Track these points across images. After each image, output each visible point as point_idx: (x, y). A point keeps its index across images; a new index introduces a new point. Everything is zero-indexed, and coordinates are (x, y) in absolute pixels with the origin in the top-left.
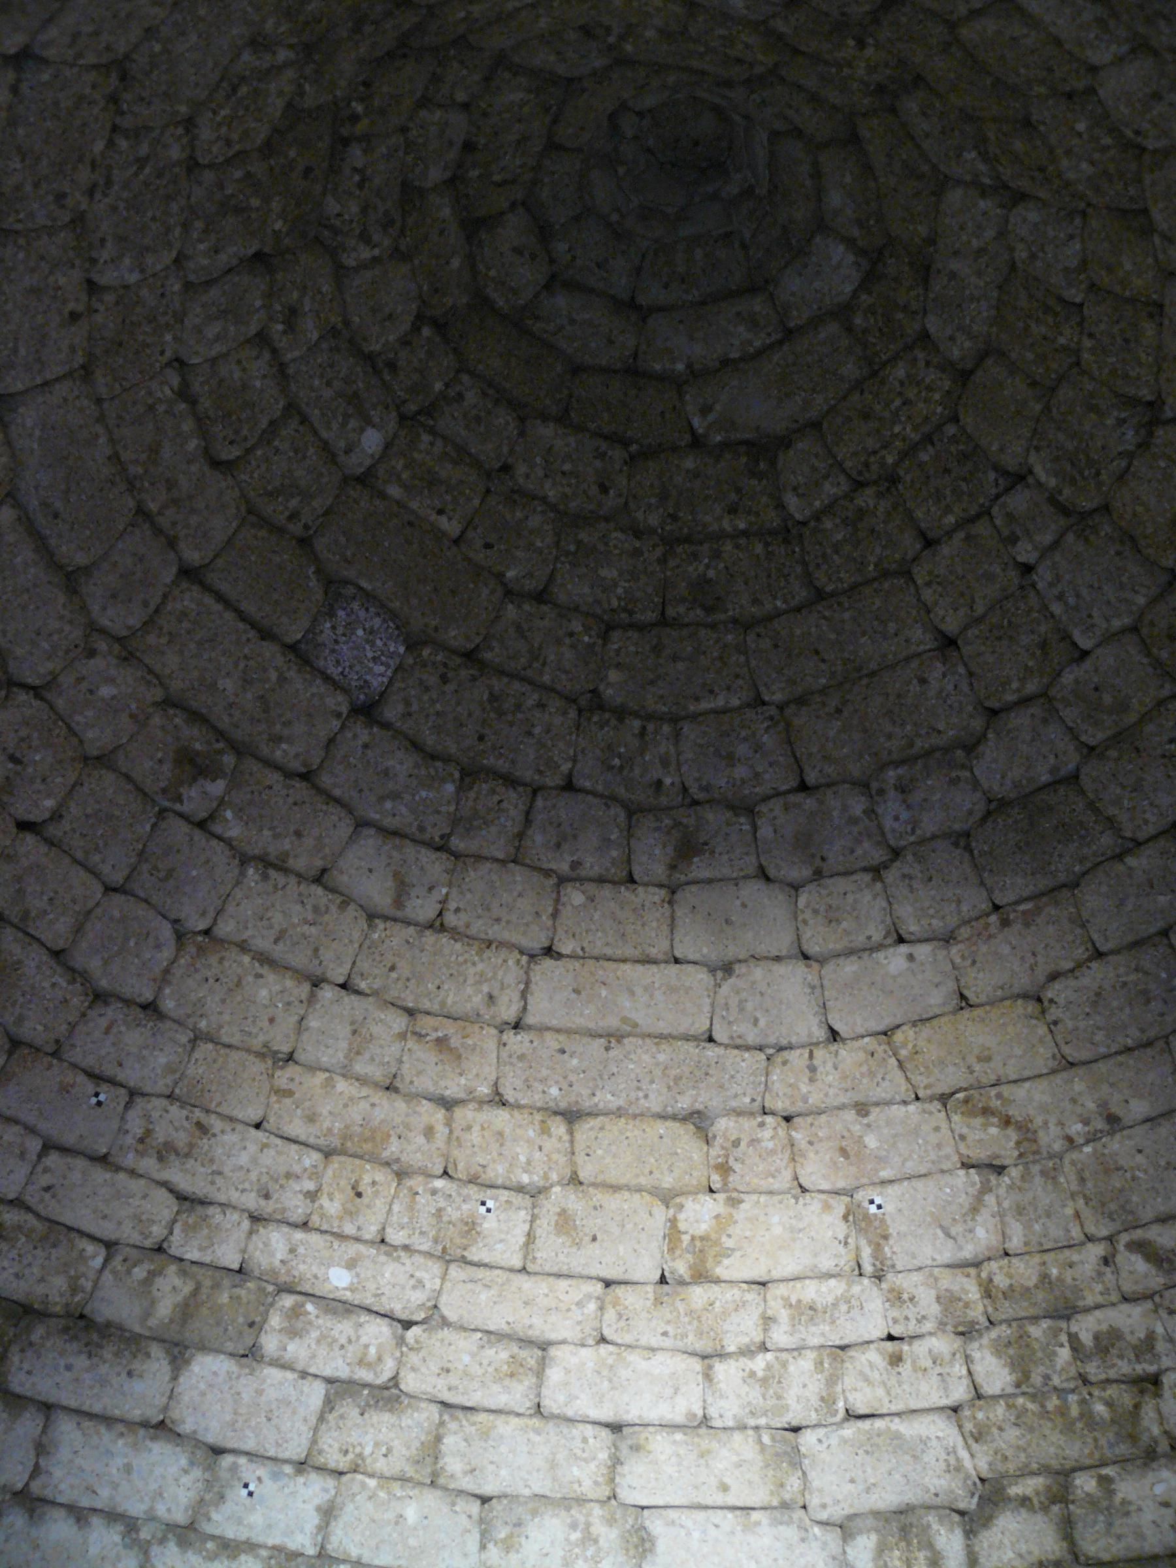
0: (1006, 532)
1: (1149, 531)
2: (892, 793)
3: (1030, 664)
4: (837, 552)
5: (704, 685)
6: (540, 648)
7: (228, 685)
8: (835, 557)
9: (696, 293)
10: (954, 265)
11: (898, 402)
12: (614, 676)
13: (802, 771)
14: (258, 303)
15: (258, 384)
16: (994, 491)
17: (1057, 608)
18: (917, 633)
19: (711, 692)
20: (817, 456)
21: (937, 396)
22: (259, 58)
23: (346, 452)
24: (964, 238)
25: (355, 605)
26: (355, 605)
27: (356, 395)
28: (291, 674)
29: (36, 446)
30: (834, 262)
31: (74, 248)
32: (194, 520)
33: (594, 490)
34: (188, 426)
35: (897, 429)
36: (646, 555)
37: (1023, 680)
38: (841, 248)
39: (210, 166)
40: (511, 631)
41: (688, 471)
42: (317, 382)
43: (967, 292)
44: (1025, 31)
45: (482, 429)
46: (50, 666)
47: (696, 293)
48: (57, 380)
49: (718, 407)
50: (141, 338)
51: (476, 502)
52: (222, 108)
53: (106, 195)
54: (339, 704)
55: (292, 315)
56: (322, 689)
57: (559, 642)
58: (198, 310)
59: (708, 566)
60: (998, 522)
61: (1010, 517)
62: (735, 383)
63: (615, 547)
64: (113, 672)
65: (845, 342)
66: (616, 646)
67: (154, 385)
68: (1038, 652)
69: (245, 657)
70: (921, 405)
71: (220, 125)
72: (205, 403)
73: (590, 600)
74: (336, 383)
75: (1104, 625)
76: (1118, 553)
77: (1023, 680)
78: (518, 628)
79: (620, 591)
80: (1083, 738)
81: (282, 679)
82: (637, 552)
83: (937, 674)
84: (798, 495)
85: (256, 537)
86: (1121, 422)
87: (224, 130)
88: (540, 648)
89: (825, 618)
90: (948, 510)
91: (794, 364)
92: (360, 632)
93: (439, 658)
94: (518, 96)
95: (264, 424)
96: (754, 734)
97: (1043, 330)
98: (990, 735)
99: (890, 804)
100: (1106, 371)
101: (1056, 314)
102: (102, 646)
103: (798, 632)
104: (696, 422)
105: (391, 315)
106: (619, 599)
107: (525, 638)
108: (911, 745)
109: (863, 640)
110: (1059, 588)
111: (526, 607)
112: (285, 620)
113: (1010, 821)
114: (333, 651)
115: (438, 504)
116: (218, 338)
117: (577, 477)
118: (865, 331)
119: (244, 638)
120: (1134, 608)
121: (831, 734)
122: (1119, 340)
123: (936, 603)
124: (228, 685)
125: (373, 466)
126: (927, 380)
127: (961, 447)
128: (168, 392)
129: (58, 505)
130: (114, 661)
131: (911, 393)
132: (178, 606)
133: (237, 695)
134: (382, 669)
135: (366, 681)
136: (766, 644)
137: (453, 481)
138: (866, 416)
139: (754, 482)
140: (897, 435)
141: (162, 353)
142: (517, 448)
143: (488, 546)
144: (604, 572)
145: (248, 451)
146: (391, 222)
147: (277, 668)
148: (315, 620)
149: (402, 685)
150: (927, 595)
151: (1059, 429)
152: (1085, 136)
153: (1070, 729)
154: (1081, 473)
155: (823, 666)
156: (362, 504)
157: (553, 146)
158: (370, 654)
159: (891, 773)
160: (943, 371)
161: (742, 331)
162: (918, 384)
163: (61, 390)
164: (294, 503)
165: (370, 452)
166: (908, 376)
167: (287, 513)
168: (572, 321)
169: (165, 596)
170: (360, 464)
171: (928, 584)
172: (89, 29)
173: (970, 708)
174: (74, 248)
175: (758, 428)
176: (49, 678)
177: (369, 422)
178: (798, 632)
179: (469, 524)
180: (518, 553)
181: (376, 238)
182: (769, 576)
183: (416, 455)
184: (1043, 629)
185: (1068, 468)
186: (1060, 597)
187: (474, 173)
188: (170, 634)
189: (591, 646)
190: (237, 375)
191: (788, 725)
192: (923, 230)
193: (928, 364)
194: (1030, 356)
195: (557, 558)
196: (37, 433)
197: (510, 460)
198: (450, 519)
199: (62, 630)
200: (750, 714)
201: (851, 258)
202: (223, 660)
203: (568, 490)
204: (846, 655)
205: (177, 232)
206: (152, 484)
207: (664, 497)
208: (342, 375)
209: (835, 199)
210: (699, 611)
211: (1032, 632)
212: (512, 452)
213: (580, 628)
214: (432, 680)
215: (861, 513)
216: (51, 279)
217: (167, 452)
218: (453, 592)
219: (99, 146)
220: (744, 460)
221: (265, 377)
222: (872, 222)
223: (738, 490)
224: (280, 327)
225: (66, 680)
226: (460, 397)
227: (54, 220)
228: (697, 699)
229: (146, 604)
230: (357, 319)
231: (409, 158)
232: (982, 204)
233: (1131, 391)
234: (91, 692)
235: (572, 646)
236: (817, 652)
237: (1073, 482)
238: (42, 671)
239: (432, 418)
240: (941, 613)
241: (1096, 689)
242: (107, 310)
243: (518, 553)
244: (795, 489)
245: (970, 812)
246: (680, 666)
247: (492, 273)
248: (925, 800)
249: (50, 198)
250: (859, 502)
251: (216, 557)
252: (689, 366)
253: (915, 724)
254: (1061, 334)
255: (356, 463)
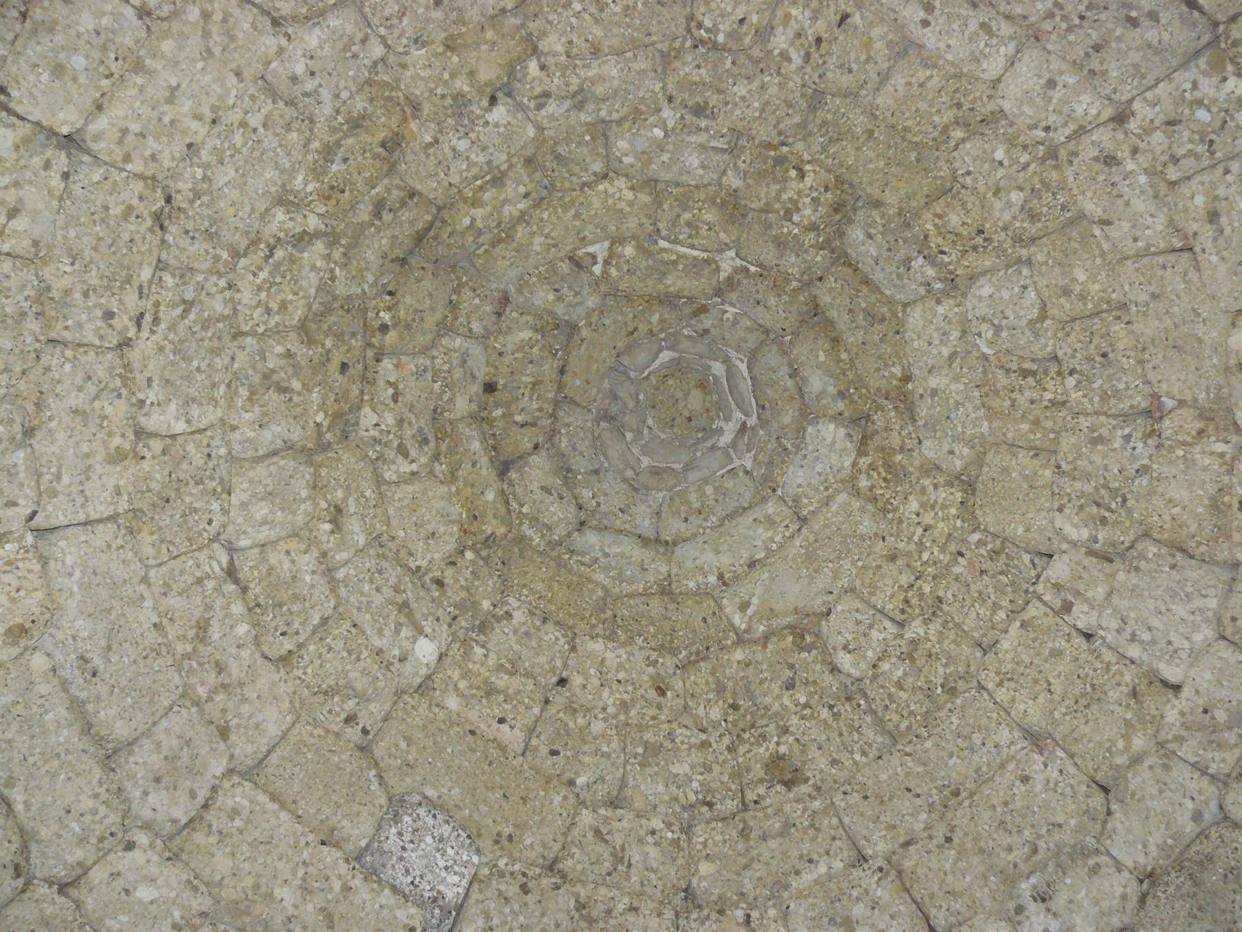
0: (1058, 604)
1: (1193, 528)
2: (1032, 907)
3: (1129, 716)
4: (902, 689)
5: (801, 857)
6: (623, 848)
7: (287, 895)
8: (901, 694)
9: (714, 519)
10: (933, 382)
11: (919, 531)
12: (705, 868)
13: (927, 919)
14: (304, 494)
15: (308, 578)
16: (1033, 573)
17: (1134, 651)
18: (1004, 735)
19: (810, 861)
20: (857, 611)
21: (953, 511)
22: (291, 219)
23: (400, 660)
24: (935, 351)
25: (422, 811)
26: (422, 811)
27: (405, 604)
28: (357, 882)
29: (75, 588)
30: (829, 440)
31: (120, 376)
32: (246, 709)
33: (652, 694)
34: (237, 609)
35: (925, 556)
36: (714, 745)
37: (1126, 737)
38: (832, 426)
39: (252, 333)
40: (590, 835)
41: (739, 662)
42: (366, 587)
43: (952, 401)
44: (928, 73)
45: (534, 644)
46: (79, 854)
47: (714, 519)
48: (99, 521)
49: (755, 601)
50: (188, 499)
51: (536, 710)
52: (261, 269)
53: (153, 332)
54: (412, 917)
55: (337, 514)
56: (392, 901)
57: (641, 841)
58: (245, 485)
59: (778, 744)
60: (1047, 598)
61: (1057, 587)
62: (766, 575)
63: (682, 743)
64: (153, 870)
65: (856, 504)
66: (701, 839)
67: (202, 556)
68: (1132, 702)
69: (304, 863)
70: (941, 525)
71: (260, 289)
72: (256, 589)
73: (667, 798)
74: (385, 590)
75: (1187, 645)
76: (1173, 567)
77: (1126, 737)
78: (597, 832)
79: (695, 784)
80: (1213, 769)
81: (347, 888)
82: (705, 745)
83: (1038, 767)
84: (849, 652)
85: (311, 735)
86: (1127, 438)
87: (264, 295)
88: (623, 848)
89: (907, 754)
90: (996, 607)
91: (816, 541)
92: (429, 840)
93: (517, 867)
94: (526, 335)
95: (316, 620)
96: (866, 891)
97: (1028, 394)
98: (1114, 807)
99: (1033, 918)
100: (1096, 399)
101: (1034, 373)
102: (142, 839)
103: (884, 777)
104: (737, 620)
105: (433, 534)
106: (696, 793)
107: (606, 841)
108: (1035, 851)
109: (951, 762)
110: (1129, 630)
111: (602, 811)
112: (345, 823)
113: (1171, 889)
114: (401, 859)
115: (497, 713)
116: (265, 522)
117: (633, 684)
118: (871, 489)
119: (303, 841)
120: (1210, 614)
121: (948, 866)
122: (1098, 359)
123: (1013, 700)
124: (287, 895)
125: (429, 677)
126: (940, 501)
127: (989, 547)
128: (217, 569)
129: (97, 661)
130: (155, 858)
131: (928, 519)
132: (230, 803)
133: (297, 907)
134: (456, 879)
135: (439, 892)
136: (855, 798)
137: (511, 691)
138: (893, 558)
139: (805, 655)
140: (926, 563)
141: (210, 522)
142: (570, 662)
143: (554, 753)
144: (676, 769)
145: (300, 646)
146: (425, 441)
147: (339, 877)
148: (380, 827)
149: (480, 897)
150: (1002, 695)
151: (1074, 479)
152: (1006, 163)
153: (1194, 766)
154: (1109, 510)
155: (918, 801)
156: (421, 710)
157: (563, 400)
158: (442, 864)
159: (1024, 886)
160: (952, 486)
161: (762, 533)
162: (933, 507)
163: (104, 533)
164: (350, 704)
165: (425, 661)
166: (922, 505)
167: (343, 716)
168: (606, 555)
169: (214, 789)
170: (416, 674)
171: (1000, 684)
172: (135, 127)
173: (1084, 788)
174: (120, 376)
175: (796, 609)
176: (79, 871)
177: (420, 631)
178: (884, 777)
179: (531, 731)
180: (587, 759)
181: (413, 453)
182: (841, 735)
183: (470, 666)
184: (1127, 678)
185: (1095, 509)
186: (1133, 638)
187: (498, 412)
188: (220, 832)
189: (675, 843)
190: (287, 565)
191: (900, 873)
192: (897, 371)
193: (936, 486)
194: (1025, 427)
195: (626, 763)
196: (78, 574)
197: (564, 675)
198: (512, 728)
199: (94, 812)
200: (857, 873)
201: (842, 432)
202: (280, 865)
203: (625, 696)
204: (939, 783)
205: (222, 389)
206: (201, 665)
207: (721, 689)
208: (390, 583)
209: (816, 383)
210: (779, 788)
211: (1119, 685)
212: (565, 665)
213: (662, 825)
214: (512, 890)
215: (914, 643)
216: (97, 404)
217: (215, 632)
218: (524, 800)
219: (146, 273)
220: (790, 639)
221: (314, 572)
222: (852, 391)
223: (791, 666)
224: (328, 527)
225: (97, 875)
226: (509, 615)
227: (101, 338)
228: (797, 873)
229: (193, 795)
230: (402, 534)
231: (437, 386)
232: (940, 310)
233: (1125, 405)
234: (127, 892)
235: (656, 844)
236: (909, 790)
237: (1104, 521)
238: (70, 859)
239: (485, 634)
240: (1022, 707)
241: (1205, 711)
242: (154, 457)
243: (587, 759)
244: (845, 647)
245: (1124, 897)
246: (773, 844)
247: (525, 510)
248: (1071, 901)
249: (99, 313)
250: (909, 635)
251: (269, 752)
252: (721, 577)
253: (1033, 826)
254: (1045, 390)
255: (412, 674)
